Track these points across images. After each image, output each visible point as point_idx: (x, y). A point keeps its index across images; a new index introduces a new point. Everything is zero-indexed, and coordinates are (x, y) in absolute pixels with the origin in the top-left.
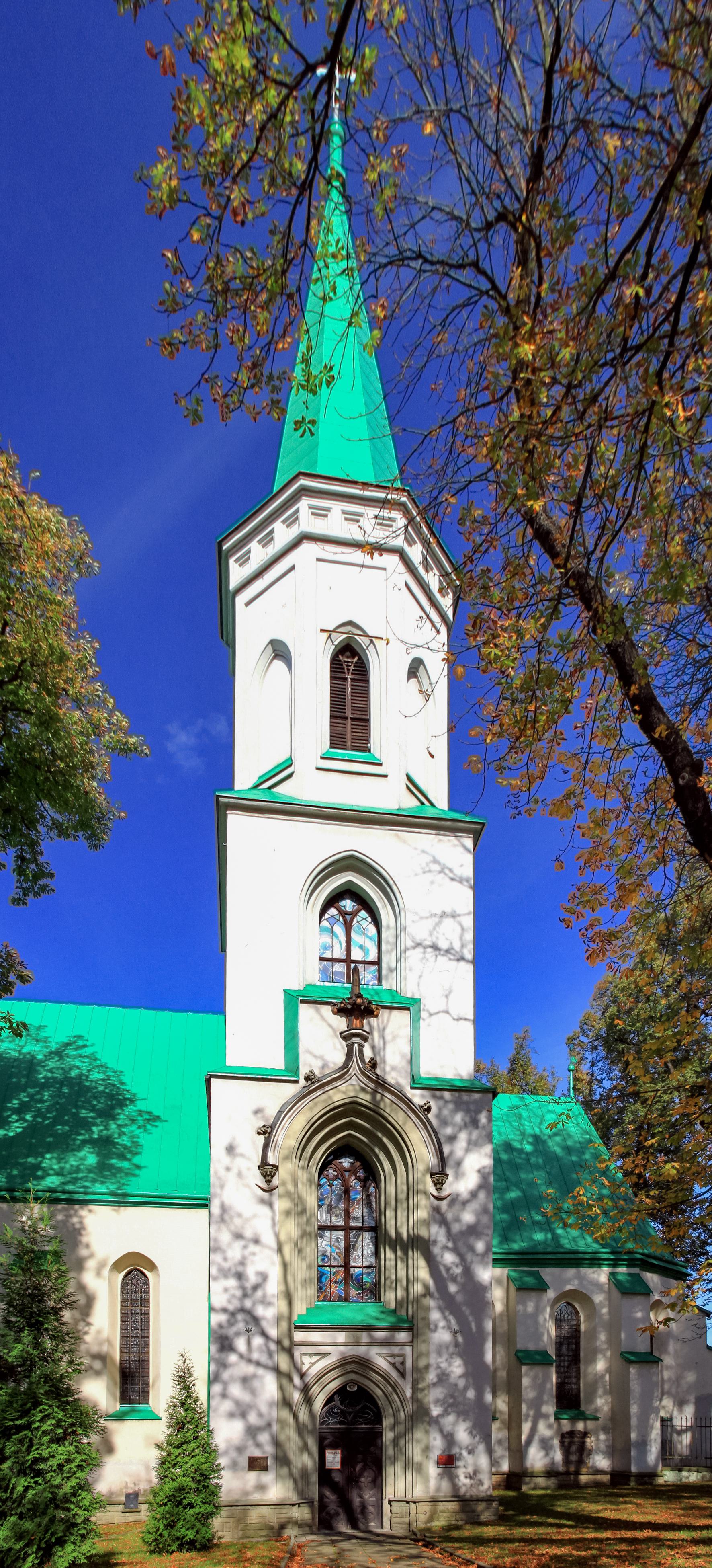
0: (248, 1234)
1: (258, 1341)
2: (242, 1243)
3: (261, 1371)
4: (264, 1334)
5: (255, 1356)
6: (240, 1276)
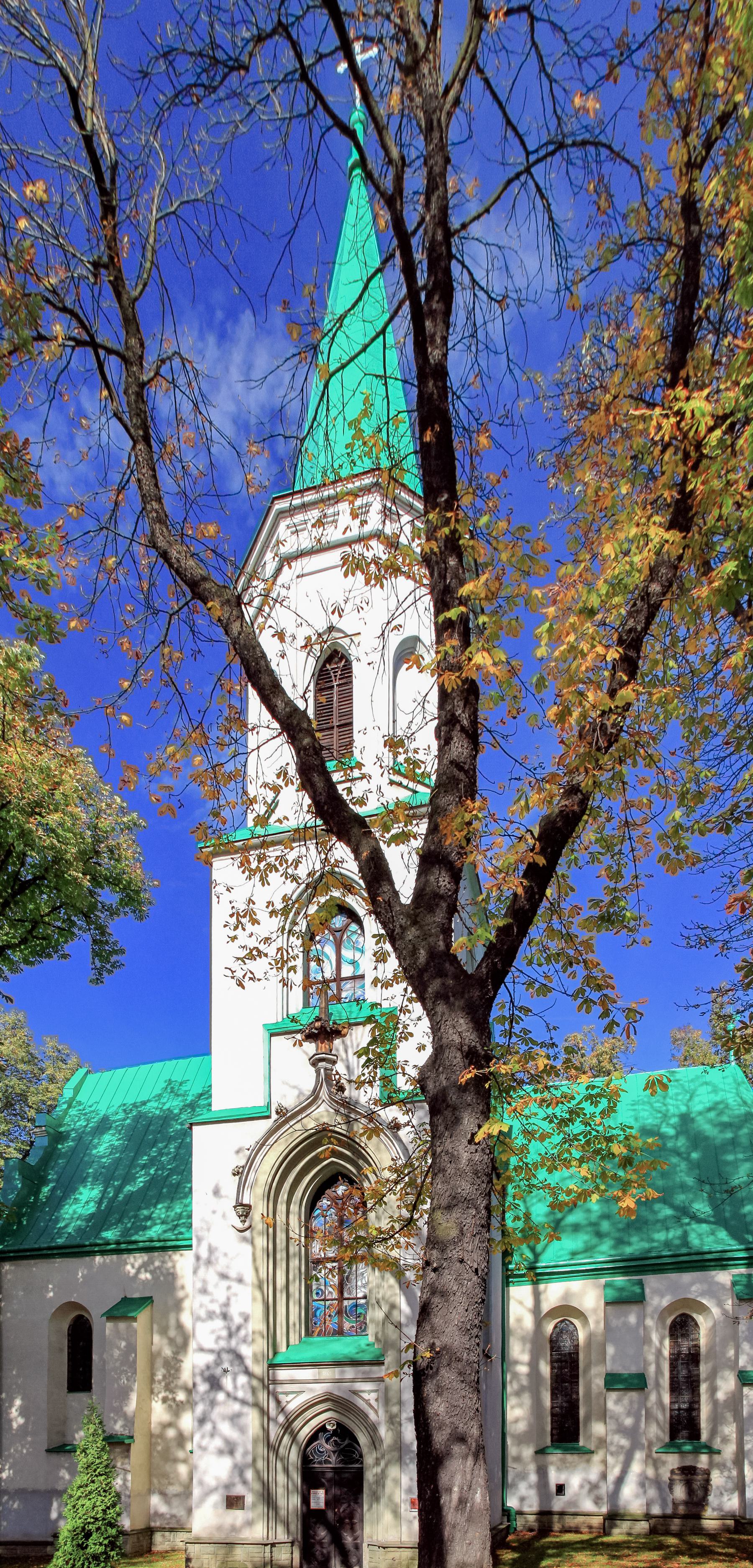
0: (233, 1274)
1: (242, 1379)
2: (225, 1283)
3: (246, 1409)
4: (247, 1372)
5: (240, 1394)
6: (225, 1316)
